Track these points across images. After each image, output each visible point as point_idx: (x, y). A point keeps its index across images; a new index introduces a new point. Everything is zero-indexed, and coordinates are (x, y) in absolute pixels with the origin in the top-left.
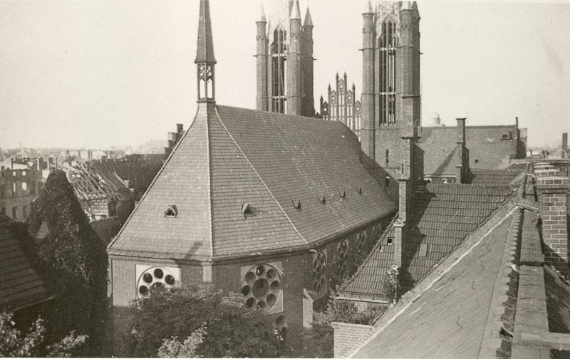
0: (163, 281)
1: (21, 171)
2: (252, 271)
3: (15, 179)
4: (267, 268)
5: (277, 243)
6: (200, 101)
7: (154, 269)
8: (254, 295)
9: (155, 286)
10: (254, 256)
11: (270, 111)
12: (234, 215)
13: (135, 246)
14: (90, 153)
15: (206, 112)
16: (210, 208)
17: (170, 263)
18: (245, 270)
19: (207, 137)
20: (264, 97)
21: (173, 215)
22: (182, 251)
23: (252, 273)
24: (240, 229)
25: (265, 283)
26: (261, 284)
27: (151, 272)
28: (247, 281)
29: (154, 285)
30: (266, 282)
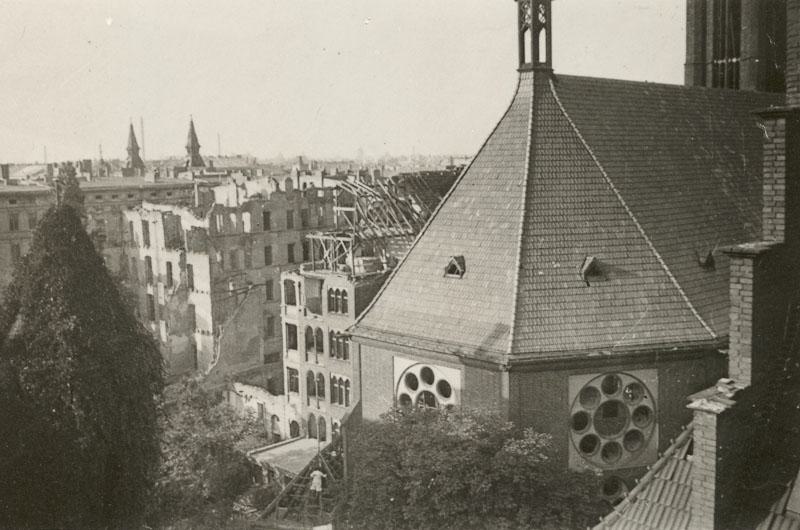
0: (433, 389)
1: (331, 189)
2: (592, 384)
3: (323, 201)
4: (626, 381)
5: (648, 334)
6: (523, 68)
7: (420, 367)
8: (596, 429)
9: (423, 397)
10: (593, 359)
11: (709, 84)
12: (564, 278)
13: (711, 275)
14: (452, 159)
15: (532, 87)
16: (518, 263)
17: (448, 361)
18: (577, 383)
19: (529, 132)
20: (696, 63)
21: (458, 273)
22: (470, 343)
23: (594, 390)
24: (574, 305)
25: (620, 410)
26: (611, 410)
27: (417, 371)
28: (583, 402)
29: (421, 394)
30: (624, 407)
